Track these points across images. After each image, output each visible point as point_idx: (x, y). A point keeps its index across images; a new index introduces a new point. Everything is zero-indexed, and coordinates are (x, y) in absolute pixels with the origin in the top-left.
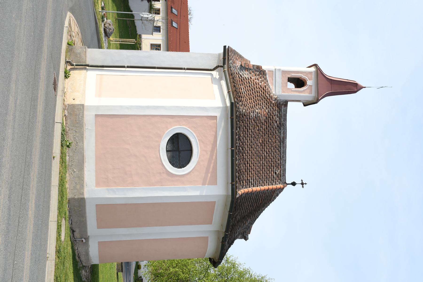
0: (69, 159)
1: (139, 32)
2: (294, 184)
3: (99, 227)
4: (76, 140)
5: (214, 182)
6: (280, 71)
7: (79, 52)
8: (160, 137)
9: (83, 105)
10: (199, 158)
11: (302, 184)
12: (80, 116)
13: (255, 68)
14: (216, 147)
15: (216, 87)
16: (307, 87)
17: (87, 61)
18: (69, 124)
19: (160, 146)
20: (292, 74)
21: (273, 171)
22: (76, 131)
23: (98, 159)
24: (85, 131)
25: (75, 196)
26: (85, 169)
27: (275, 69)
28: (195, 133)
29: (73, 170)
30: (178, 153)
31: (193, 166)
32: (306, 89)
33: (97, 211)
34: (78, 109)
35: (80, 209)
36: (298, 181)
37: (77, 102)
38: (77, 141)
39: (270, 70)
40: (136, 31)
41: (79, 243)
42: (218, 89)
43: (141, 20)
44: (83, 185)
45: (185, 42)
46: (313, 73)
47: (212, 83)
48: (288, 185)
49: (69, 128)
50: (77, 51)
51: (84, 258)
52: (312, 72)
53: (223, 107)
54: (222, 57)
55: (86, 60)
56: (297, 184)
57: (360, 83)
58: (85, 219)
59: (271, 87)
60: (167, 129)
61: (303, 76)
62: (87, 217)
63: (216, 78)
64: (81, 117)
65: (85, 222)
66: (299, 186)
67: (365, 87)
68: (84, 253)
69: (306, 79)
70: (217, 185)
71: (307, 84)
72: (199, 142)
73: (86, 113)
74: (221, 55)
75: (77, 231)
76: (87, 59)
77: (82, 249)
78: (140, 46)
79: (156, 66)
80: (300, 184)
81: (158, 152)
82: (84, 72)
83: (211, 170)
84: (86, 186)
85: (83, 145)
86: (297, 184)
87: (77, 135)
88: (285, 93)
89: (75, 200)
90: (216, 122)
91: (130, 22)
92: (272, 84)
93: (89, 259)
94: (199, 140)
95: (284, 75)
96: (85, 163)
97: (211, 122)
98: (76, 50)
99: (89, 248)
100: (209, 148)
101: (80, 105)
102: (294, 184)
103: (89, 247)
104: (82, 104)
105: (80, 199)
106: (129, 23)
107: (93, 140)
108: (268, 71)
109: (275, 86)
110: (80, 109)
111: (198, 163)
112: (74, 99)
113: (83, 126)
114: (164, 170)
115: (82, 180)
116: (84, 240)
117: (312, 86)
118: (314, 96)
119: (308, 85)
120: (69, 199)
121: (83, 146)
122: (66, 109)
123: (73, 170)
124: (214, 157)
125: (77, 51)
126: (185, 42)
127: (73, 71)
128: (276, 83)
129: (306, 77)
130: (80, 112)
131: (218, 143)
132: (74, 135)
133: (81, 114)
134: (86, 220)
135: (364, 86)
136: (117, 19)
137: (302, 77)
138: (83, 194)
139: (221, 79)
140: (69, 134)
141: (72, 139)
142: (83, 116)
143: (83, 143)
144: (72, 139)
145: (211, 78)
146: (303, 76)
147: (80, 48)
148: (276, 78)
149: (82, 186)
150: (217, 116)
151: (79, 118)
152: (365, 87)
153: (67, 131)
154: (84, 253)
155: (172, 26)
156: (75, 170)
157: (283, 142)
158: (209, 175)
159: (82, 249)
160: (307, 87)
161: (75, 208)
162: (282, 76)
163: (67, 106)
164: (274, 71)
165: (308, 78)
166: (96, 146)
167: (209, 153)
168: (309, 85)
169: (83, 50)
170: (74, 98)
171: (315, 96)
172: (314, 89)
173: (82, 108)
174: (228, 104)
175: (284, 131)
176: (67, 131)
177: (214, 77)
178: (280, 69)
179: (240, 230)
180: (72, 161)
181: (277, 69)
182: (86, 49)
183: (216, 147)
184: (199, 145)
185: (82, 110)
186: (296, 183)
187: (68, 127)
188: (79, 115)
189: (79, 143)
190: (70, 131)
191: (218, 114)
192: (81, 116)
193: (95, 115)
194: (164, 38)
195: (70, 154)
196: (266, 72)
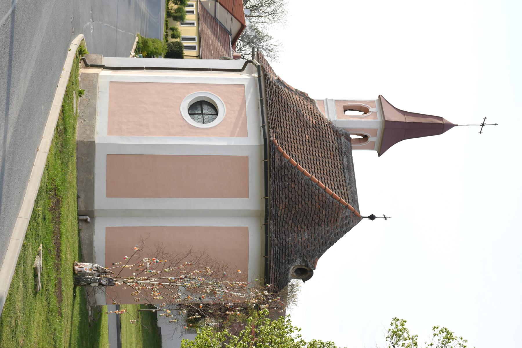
2: (372, 217)
3: (109, 195)
5: (244, 133)
7: (94, 58)
10: (226, 115)
11: (385, 218)
14: (245, 108)
19: (180, 106)
20: (349, 103)
23: (111, 114)
24: (98, 93)
25: (84, 139)
28: (220, 97)
30: (202, 115)
33: (107, 166)
35: (88, 160)
41: (82, 226)
44: (94, 131)
46: (376, 102)
48: (363, 219)
50: (92, 58)
51: (86, 251)
52: (374, 101)
56: (376, 217)
57: (449, 118)
58: (93, 176)
62: (96, 176)
65: (92, 181)
67: (457, 125)
68: (87, 242)
69: (367, 107)
70: (248, 137)
72: (225, 104)
75: (81, 197)
77: (85, 235)
81: (179, 110)
83: (240, 125)
86: (376, 217)
89: (84, 144)
90: (244, 89)
92: (324, 111)
93: (92, 254)
94: (225, 102)
95: (338, 104)
97: (238, 89)
99: (94, 235)
100: (237, 108)
102: (372, 217)
103: (94, 233)
105: (89, 142)
107: (107, 100)
110: (95, 76)
111: (224, 120)
114: (186, 124)
115: (93, 128)
116: (89, 219)
117: (376, 112)
118: (380, 121)
119: (371, 112)
120: (77, 143)
121: (96, 102)
124: (243, 115)
130: (94, 78)
131: (247, 104)
132: (87, 95)
134: (94, 178)
135: (455, 124)
136: (139, 311)
137: (362, 106)
138: (93, 138)
149: (93, 132)
150: (244, 85)
151: (92, 82)
152: (457, 125)
154: (87, 242)
158: (238, 129)
159: (85, 235)
161: (83, 157)
162: (336, 104)
164: (325, 100)
165: (370, 106)
167: (237, 112)
168: (373, 112)
171: (381, 120)
173: (96, 75)
179: (304, 276)
181: (328, 99)
182: (102, 56)
183: (245, 108)
184: (225, 106)
186: (376, 216)
188: (93, 80)
189: (91, 101)
192: (95, 81)
193: (110, 82)
195: (81, 108)
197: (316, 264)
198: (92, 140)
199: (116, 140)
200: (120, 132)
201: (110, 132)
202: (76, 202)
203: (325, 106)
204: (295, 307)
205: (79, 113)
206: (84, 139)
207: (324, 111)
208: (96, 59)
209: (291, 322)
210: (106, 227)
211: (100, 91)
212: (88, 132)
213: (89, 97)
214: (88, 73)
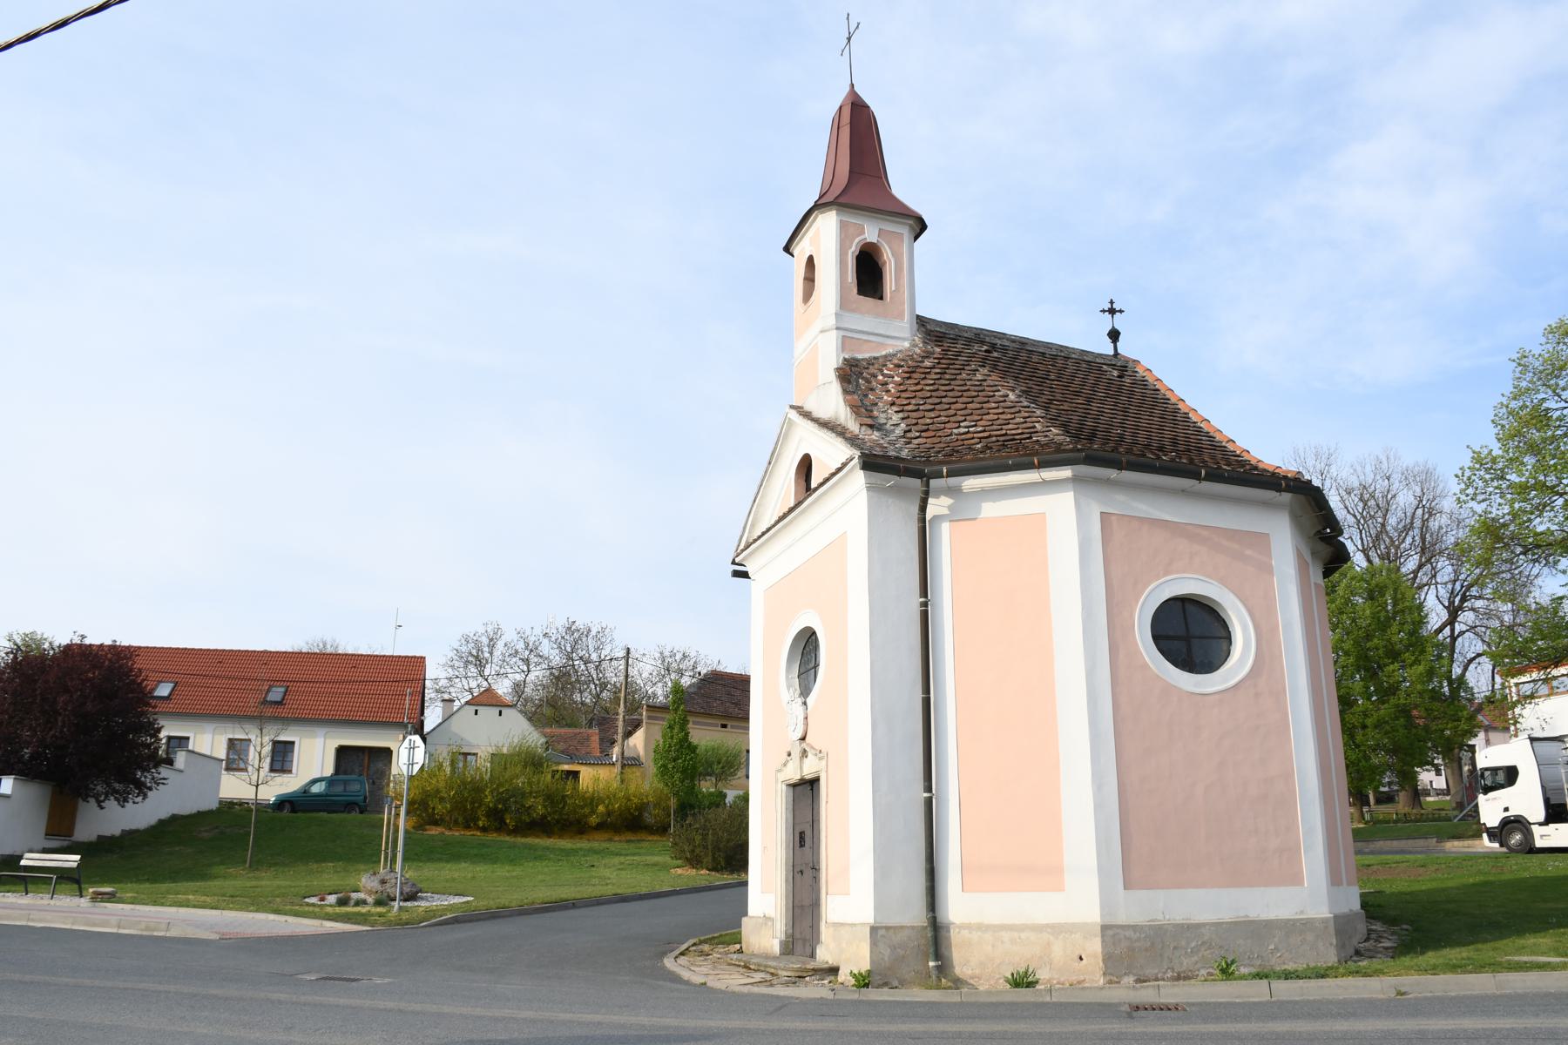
0: (1245, 966)
1: (214, 805)
2: (1114, 335)
4: (1197, 945)
6: (841, 315)
7: (889, 950)
8: (1169, 689)
9: (1105, 928)
12: (1134, 936)
13: (851, 388)
15: (990, 509)
16: (883, 243)
17: (915, 925)
18: (1156, 971)
20: (850, 280)
21: (984, 405)
22: (1175, 948)
23: (1237, 878)
25: (1331, 944)
26: (1264, 916)
27: (837, 328)
29: (1272, 953)
31: (1232, 596)
32: (890, 248)
34: (1114, 944)
36: (1106, 323)
37: (1095, 947)
38: (1199, 943)
39: (840, 346)
40: (210, 812)
42: (998, 503)
43: (257, 786)
45: (221, 662)
47: (975, 519)
49: (1169, 968)
50: (886, 959)
53: (1075, 492)
54: (892, 480)
55: (913, 928)
59: (890, 350)
60: (1146, 666)
61: (853, 248)
63: (949, 507)
64: (1135, 933)
66: (1119, 322)
70: (1268, 534)
71: (876, 242)
73: (1122, 918)
74: (874, 482)
76: (909, 925)
78: (236, 804)
79: (919, 695)
80: (1113, 317)
82: (959, 932)
84: (1302, 912)
85: (1207, 924)
87: (1183, 943)
88: (904, 311)
91: (202, 829)
92: (883, 345)
96: (1248, 916)
98: (883, 959)
101: (1103, 936)
102: (1114, 335)
104: (1102, 931)
106: (206, 831)
108: (843, 351)
109: (888, 337)
110: (1114, 935)
111: (1223, 582)
112: (1081, 959)
113: (1160, 927)
122: (1117, 980)
123: (1272, 953)
124: (1205, 533)
125: (886, 959)
126: (221, 662)
127: (954, 968)
128: (876, 332)
129: (857, 240)
133: (1127, 934)
135: (847, 89)
138: (1325, 921)
139: (953, 492)
140: (1184, 968)
141: (1196, 958)
142: (1134, 928)
143: (1204, 925)
144: (1196, 958)
145: (950, 521)
146: (853, 250)
147: (877, 946)
148: (865, 330)
152: (852, 85)
153: (1176, 975)
155: (167, 698)
156: (1272, 947)
157: (1023, 344)
158: (1248, 552)
160: (883, 243)
163: (1108, 978)
164: (842, 333)
166: (1203, 886)
169: (883, 936)
170: (1077, 954)
171: (908, 227)
172: (890, 227)
173: (1110, 932)
174: (1066, 472)
175: (1008, 339)
176: (1176, 975)
177: (946, 511)
178: (836, 314)
180: (1249, 957)
185: (1118, 931)
187: (1165, 973)
188: (1129, 939)
189: (1206, 938)
190: (1175, 967)
191: (1095, 510)
192: (1132, 933)
194: (209, 727)
196: (847, 357)
197: (1062, 348)
198: (1331, 924)
199: (1313, 859)
200: (1290, 852)
201: (1296, 879)
202: (1145, 984)
203: (865, 337)
204: (1438, 469)
205: (1252, 966)
206: (1331, 944)
207: (883, 345)
208: (890, 947)
209: (1457, 476)
210: (1127, 885)
211: (1162, 916)
212: (1310, 937)
213: (1193, 944)
214: (1103, 956)
